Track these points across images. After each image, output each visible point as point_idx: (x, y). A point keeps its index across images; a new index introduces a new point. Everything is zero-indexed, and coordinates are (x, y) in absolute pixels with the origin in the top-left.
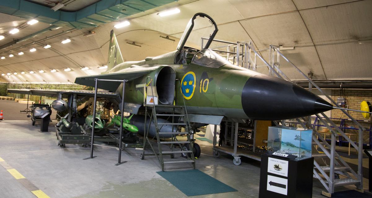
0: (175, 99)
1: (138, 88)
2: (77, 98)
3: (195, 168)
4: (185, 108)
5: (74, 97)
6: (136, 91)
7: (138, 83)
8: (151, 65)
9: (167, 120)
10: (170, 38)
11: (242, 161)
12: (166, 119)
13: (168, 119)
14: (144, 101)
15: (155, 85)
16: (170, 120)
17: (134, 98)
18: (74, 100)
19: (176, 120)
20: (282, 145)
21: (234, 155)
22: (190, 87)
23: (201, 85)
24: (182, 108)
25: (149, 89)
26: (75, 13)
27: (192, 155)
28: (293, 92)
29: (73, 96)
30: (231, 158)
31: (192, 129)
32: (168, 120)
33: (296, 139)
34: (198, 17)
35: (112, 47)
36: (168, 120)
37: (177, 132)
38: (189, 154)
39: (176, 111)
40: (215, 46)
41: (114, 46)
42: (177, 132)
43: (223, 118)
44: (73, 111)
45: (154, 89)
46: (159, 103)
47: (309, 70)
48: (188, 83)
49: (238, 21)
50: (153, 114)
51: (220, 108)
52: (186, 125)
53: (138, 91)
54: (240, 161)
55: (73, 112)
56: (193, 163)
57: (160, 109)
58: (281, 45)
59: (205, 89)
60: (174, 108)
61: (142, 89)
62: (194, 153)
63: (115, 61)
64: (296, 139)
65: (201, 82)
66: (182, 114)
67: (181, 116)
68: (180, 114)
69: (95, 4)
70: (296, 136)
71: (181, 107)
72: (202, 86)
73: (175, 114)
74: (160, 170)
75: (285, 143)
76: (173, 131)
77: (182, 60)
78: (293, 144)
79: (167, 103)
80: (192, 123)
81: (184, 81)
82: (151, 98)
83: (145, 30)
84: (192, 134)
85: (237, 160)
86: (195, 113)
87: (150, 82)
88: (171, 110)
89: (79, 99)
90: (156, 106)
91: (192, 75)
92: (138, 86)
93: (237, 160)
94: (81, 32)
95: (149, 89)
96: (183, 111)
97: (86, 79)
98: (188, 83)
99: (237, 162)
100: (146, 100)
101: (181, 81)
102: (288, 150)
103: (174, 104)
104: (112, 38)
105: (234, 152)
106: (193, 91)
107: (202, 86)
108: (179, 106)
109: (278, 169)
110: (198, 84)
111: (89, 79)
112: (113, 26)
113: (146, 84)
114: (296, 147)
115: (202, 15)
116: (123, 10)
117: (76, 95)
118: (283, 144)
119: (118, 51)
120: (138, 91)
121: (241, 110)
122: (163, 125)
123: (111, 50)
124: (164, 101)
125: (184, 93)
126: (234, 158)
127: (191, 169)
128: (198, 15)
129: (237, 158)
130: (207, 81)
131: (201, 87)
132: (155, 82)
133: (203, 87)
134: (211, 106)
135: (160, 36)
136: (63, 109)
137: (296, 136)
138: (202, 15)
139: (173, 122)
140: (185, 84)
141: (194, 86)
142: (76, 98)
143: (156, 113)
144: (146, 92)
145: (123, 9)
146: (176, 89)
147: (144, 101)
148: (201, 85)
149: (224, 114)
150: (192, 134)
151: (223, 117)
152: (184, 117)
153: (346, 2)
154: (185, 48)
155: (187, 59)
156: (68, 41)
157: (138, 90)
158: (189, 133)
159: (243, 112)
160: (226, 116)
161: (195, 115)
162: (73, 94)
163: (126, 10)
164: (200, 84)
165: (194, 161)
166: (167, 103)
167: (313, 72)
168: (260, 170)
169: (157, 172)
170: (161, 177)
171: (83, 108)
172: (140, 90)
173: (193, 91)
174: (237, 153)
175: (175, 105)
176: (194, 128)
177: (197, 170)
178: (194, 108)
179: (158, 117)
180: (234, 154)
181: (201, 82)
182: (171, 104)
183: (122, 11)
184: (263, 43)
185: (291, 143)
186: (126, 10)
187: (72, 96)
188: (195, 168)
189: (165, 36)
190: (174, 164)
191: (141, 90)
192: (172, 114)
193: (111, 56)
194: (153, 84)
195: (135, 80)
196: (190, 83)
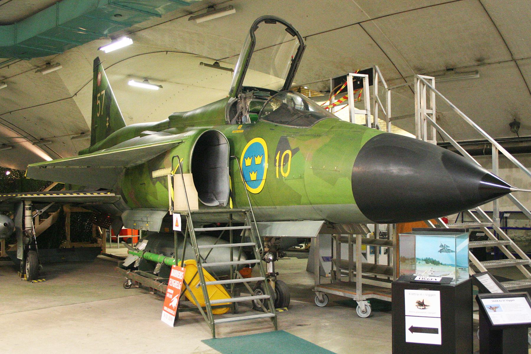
0: (232, 194)
1: (156, 178)
2: (32, 209)
3: (276, 328)
4: (251, 212)
5: (27, 206)
6: (154, 184)
7: (156, 168)
8: (181, 130)
9: (219, 238)
10: (222, 65)
11: (373, 310)
12: (218, 237)
13: (220, 236)
14: (170, 204)
15: (189, 171)
16: (224, 237)
17: (151, 198)
18: (28, 213)
19: (237, 237)
20: (417, 263)
21: (358, 298)
22: (258, 168)
23: (277, 164)
24: (246, 214)
25: (178, 178)
26: (13, 25)
27: (271, 303)
28: (442, 165)
29: (24, 205)
30: (352, 304)
31: (270, 252)
32: (221, 238)
33: (441, 251)
34: (262, 25)
35: (99, 95)
36: (221, 238)
37: (239, 260)
38: (265, 302)
39: (236, 218)
40: (317, 77)
41: (103, 92)
42: (239, 260)
43: (324, 223)
44: (28, 236)
45: (189, 178)
46: (201, 205)
47: (511, 117)
48: (253, 161)
49: (359, 23)
50: (188, 229)
51: (315, 206)
52: (254, 246)
53: (158, 185)
54: (369, 310)
55: (28, 239)
56: (273, 318)
57: (205, 218)
58: (451, 67)
59: (285, 171)
60: (231, 214)
61: (163, 179)
62: (273, 299)
63: (107, 124)
64: (441, 251)
65: (278, 158)
66: (246, 225)
67: (245, 229)
68: (242, 224)
69: (54, 7)
70: (442, 246)
71: (244, 210)
72: (280, 166)
73: (235, 224)
74: (210, 337)
75: (422, 260)
76: (232, 260)
77: (241, 114)
78: (437, 260)
79: (216, 203)
80: (270, 239)
81: (245, 158)
82: (182, 194)
83: (167, 51)
84: (271, 263)
85: (363, 308)
86: (272, 219)
87: (179, 165)
88: (226, 218)
89: (37, 211)
90: (193, 213)
91: (258, 145)
92: (156, 174)
93: (363, 308)
94: (31, 65)
95: (178, 178)
96: (247, 220)
97: (48, 167)
98: (253, 161)
99: (363, 312)
100: (173, 203)
101: (239, 159)
102: (431, 271)
103: (231, 206)
104: (97, 76)
105: (357, 291)
106: (264, 177)
107: (280, 166)
108: (240, 210)
109: (423, 314)
110: (272, 161)
111: (56, 167)
112: (99, 49)
113: (171, 169)
114: (442, 264)
115: (271, 20)
116: (115, 16)
117: (29, 203)
118: (419, 263)
119: (112, 102)
120: (158, 185)
121: (353, 206)
122: (212, 249)
123: (99, 102)
124: (211, 201)
125: (247, 181)
126: (357, 304)
127: (269, 330)
128: (262, 21)
129: (363, 306)
130: (287, 156)
131: (277, 168)
132: (188, 162)
133: (282, 167)
134: (299, 204)
135: (201, 63)
136: (4, 234)
137: (442, 246)
138: (271, 20)
139: (231, 239)
140: (248, 162)
141: (266, 165)
142: (30, 209)
143: (194, 227)
144: (173, 187)
145: (115, 14)
146: (231, 174)
147: (170, 204)
148: (277, 164)
149: (325, 217)
150: (271, 263)
151: (323, 222)
152: (250, 229)
153: (439, 3)
154: (246, 89)
155: (250, 112)
156: (125, 42)
157: (158, 182)
158: (264, 260)
159: (357, 209)
160: (328, 219)
161: (269, 223)
162: (24, 202)
163: (121, 15)
164: (275, 160)
165: (273, 315)
166: (216, 203)
167: (519, 119)
168: (391, 317)
169: (203, 341)
170: (210, 348)
171: (49, 226)
172: (161, 182)
173: (264, 177)
174: (363, 294)
175: (233, 207)
176: (273, 250)
177: (282, 331)
178: (267, 209)
179: (199, 235)
180: (357, 295)
181: (278, 158)
182: (225, 205)
183: (114, 18)
184: (414, 66)
185: (434, 259)
186: (121, 15)
187: (22, 204)
188: (276, 328)
189: (212, 63)
190: (233, 323)
191: (163, 182)
192: (229, 226)
193: (98, 115)
194: (185, 169)
195: (149, 161)
196: (258, 160)
